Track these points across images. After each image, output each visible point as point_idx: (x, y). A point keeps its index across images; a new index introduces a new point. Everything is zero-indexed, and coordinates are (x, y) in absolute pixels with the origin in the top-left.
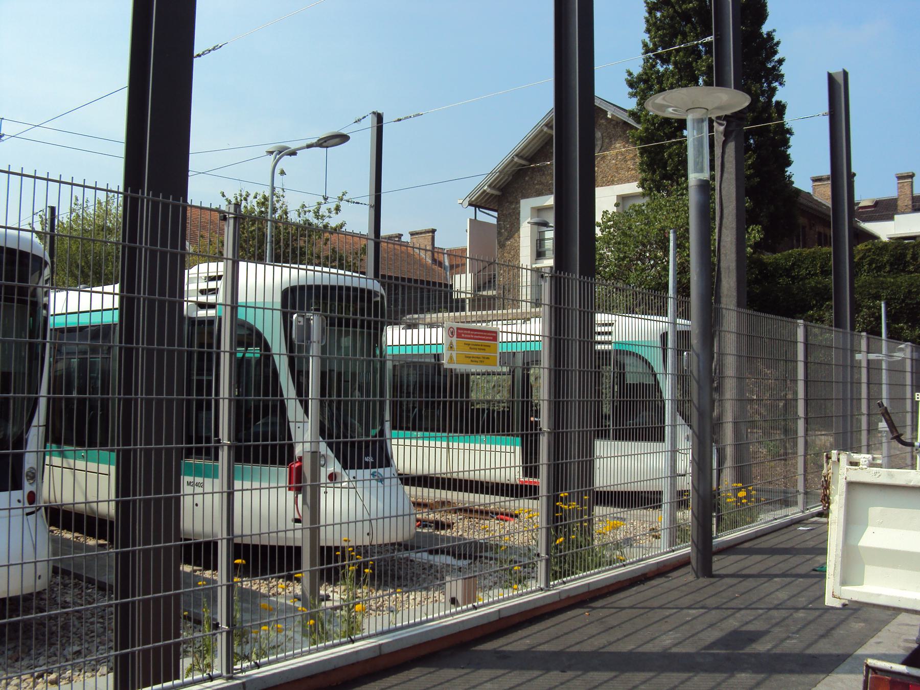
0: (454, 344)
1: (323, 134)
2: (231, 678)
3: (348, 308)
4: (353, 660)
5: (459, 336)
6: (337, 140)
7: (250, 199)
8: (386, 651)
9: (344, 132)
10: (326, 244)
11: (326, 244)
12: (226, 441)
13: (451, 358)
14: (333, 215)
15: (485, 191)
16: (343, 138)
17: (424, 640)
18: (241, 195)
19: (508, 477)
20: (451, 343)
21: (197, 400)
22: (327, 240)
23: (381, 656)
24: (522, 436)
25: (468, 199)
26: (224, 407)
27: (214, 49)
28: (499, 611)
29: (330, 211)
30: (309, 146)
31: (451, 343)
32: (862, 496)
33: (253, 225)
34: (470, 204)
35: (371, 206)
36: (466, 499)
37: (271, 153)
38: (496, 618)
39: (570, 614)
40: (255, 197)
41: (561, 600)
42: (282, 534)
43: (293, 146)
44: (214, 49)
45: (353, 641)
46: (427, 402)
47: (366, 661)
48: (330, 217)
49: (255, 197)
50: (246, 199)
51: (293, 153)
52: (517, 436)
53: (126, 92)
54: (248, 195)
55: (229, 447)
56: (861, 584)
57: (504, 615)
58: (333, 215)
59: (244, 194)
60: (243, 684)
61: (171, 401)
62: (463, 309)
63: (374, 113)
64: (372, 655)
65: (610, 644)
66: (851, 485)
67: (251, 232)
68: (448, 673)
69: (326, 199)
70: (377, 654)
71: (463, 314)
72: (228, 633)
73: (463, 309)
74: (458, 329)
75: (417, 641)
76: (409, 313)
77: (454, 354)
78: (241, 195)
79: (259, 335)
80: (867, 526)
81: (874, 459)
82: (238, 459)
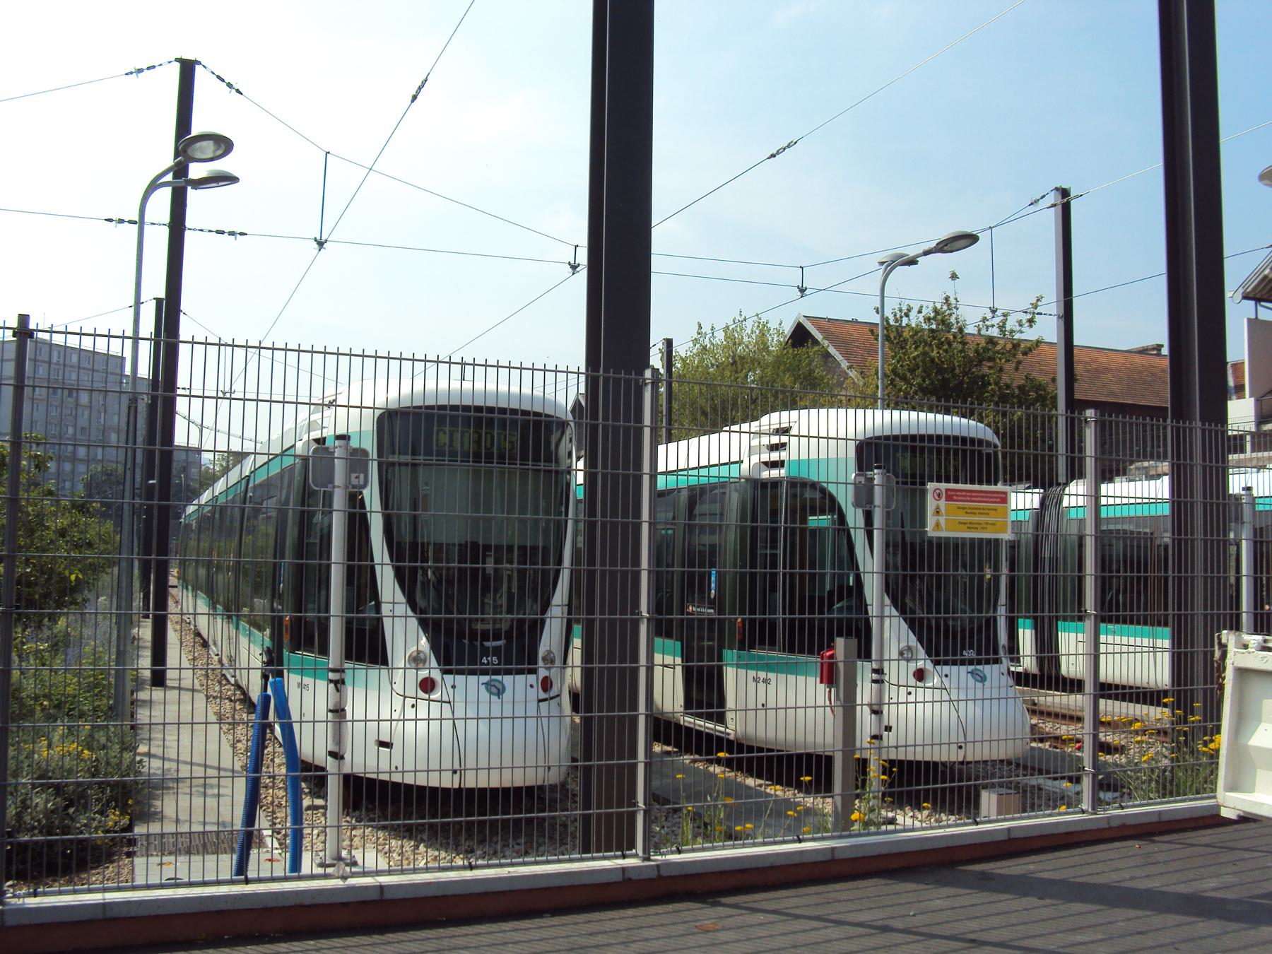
0: (943, 508)
1: (944, 235)
2: (649, 859)
3: (1124, 451)
4: (797, 860)
5: (949, 498)
6: (963, 242)
7: (913, 314)
8: (839, 856)
9: (968, 230)
10: (1017, 369)
11: (1017, 369)
12: (645, 614)
13: (938, 525)
14: (1025, 328)
15: (1266, 277)
16: (971, 239)
17: (895, 850)
18: (901, 310)
19: (1159, 679)
20: (938, 507)
21: (810, 574)
22: (1019, 363)
23: (833, 861)
24: (1035, 618)
25: (1241, 290)
26: (644, 576)
27: (789, 146)
28: (1009, 829)
29: (1020, 324)
30: (926, 253)
31: (938, 507)
32: (1256, 686)
33: (916, 348)
34: (1246, 297)
35: (1059, 317)
36: (1117, 710)
37: (882, 263)
38: (1004, 837)
39: (1117, 844)
40: (920, 312)
41: (1111, 828)
42: (919, 749)
43: (911, 252)
44: (789, 146)
45: (800, 841)
46: (1139, 578)
47: (815, 864)
48: (1021, 332)
49: (920, 312)
50: (907, 315)
51: (912, 262)
52: (1029, 617)
53: (655, 220)
54: (909, 310)
55: (649, 620)
56: (1252, 791)
57: (1014, 835)
58: (1025, 328)
59: (905, 308)
60: (658, 866)
61: (931, 576)
62: (1242, 450)
63: (1057, 189)
64: (821, 858)
65: (1132, 878)
66: (1242, 672)
67: (914, 358)
68: (910, 886)
69: (994, 311)
70: (828, 857)
71: (1242, 456)
72: (645, 812)
73: (1242, 450)
74: (947, 490)
75: (884, 851)
76: (1235, 452)
77: (942, 520)
78: (901, 310)
79: (833, 499)
80: (1260, 721)
81: (1265, 641)
82: (659, 633)
